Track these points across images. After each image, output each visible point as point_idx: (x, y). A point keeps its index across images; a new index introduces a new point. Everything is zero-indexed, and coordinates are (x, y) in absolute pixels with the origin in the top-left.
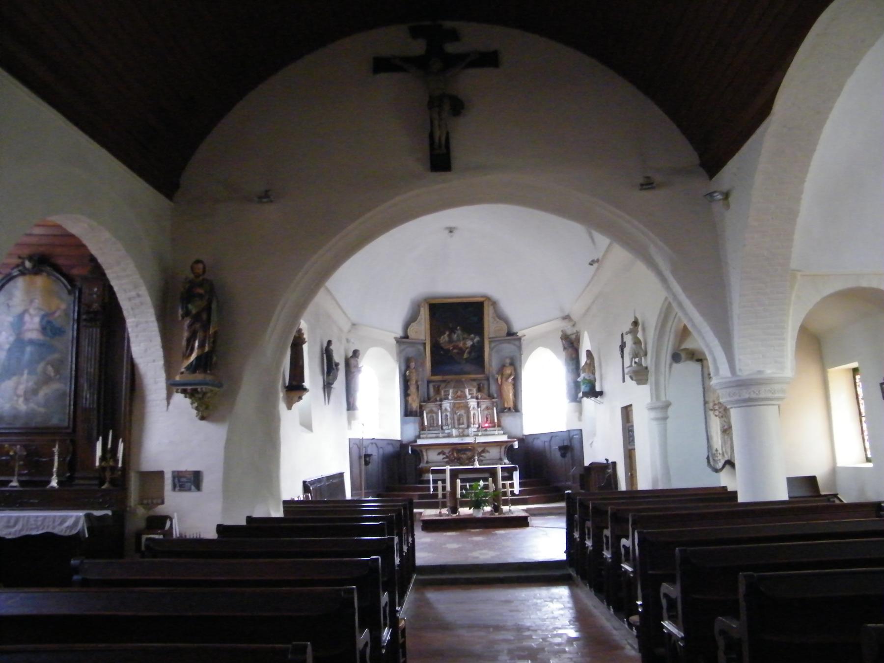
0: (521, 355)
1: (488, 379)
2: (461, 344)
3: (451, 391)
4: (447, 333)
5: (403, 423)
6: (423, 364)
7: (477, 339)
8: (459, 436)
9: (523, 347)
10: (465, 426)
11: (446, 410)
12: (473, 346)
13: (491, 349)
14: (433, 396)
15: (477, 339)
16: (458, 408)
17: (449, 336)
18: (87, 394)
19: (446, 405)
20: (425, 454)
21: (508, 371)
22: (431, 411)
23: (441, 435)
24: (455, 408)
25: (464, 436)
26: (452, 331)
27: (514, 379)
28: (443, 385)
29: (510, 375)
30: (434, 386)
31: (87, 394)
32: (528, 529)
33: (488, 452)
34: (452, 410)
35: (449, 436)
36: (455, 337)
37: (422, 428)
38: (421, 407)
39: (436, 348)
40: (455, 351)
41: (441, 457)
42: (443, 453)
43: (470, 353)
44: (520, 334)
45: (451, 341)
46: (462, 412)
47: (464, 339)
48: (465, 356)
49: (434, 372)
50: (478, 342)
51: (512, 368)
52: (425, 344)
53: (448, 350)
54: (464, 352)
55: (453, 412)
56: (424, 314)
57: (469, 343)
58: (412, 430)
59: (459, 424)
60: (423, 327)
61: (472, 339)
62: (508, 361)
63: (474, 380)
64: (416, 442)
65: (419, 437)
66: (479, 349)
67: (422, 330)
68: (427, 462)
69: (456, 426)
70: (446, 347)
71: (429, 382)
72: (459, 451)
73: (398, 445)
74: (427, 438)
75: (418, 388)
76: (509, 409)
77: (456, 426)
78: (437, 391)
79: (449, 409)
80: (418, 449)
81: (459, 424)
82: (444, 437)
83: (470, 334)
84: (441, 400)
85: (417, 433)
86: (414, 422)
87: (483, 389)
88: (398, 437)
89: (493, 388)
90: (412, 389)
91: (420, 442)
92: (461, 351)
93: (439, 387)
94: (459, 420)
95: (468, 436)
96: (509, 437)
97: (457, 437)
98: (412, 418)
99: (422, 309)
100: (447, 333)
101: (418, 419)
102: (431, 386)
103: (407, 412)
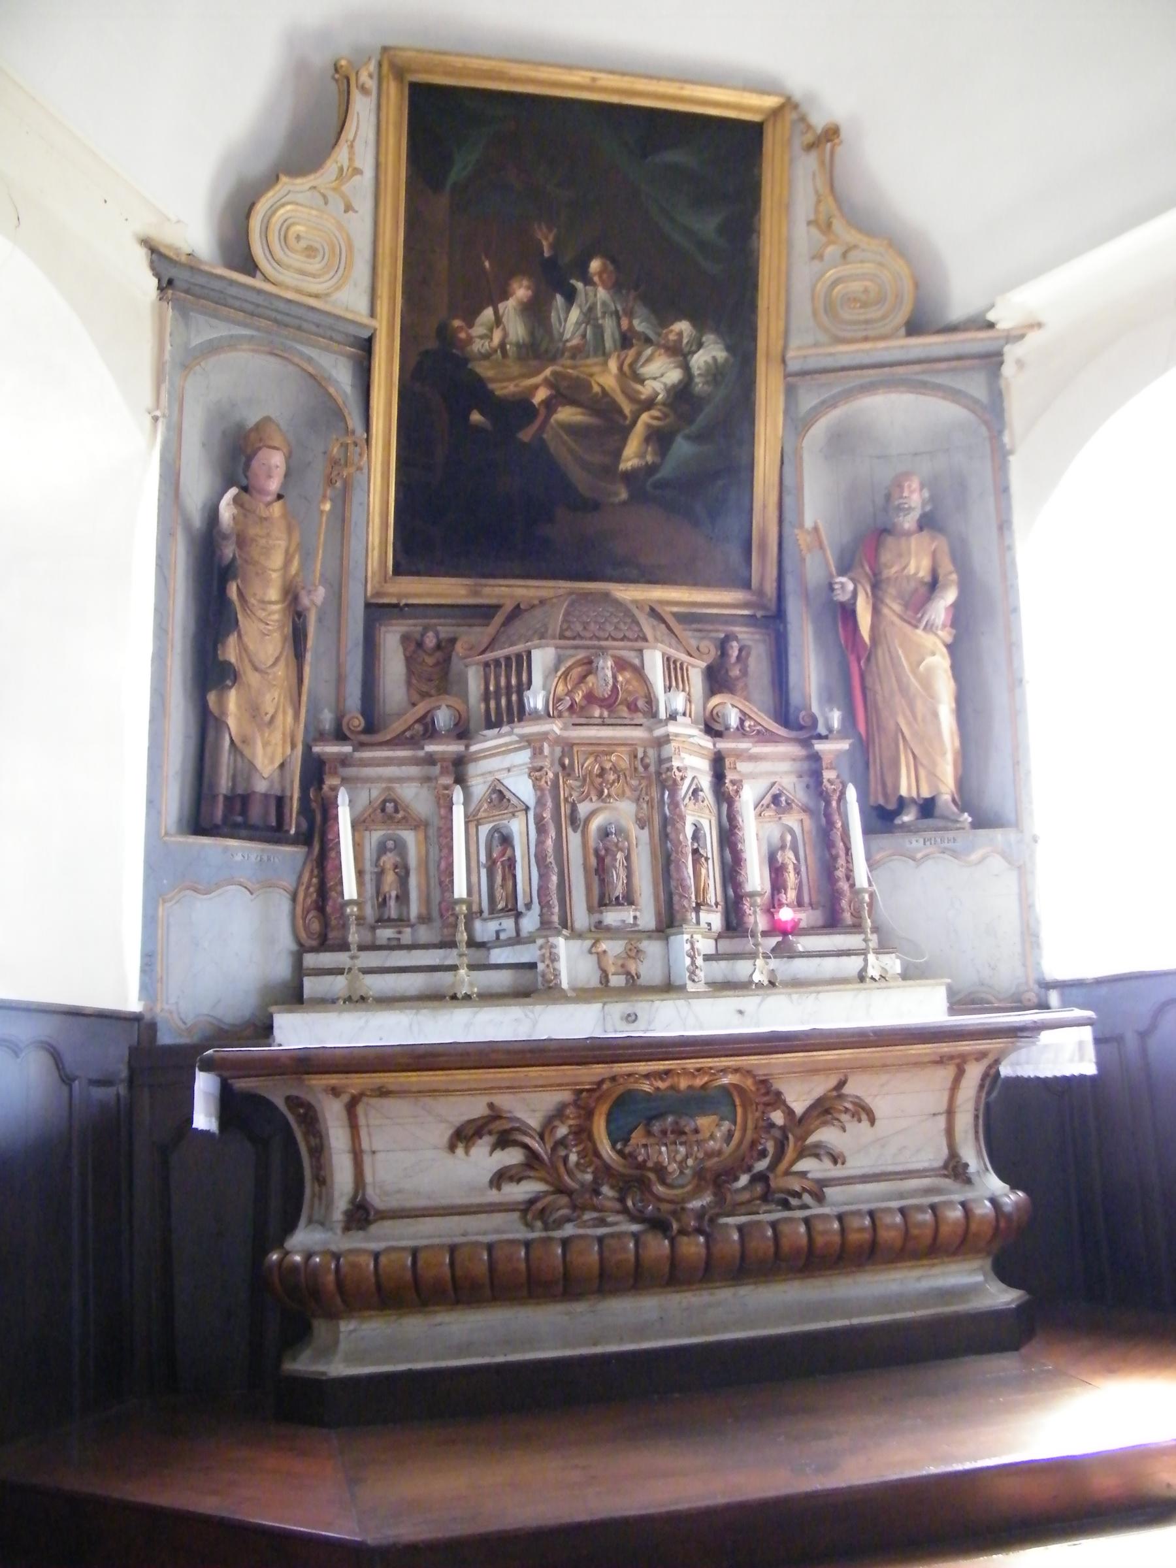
0: (1000, 456)
1: (773, 620)
2: (606, 377)
3: (542, 658)
4: (521, 291)
5: (164, 882)
6: (342, 483)
7: (711, 353)
8: (600, 991)
9: (1017, 407)
10: (646, 915)
11: (500, 797)
12: (682, 394)
13: (798, 424)
14: (432, 697)
15: (711, 353)
16: (599, 785)
17: (535, 311)
18: (445, 1059)
19: (506, 763)
20: (338, 1138)
21: (915, 560)
22: (388, 811)
23: (466, 980)
24: (570, 777)
25: (634, 987)
26: (557, 279)
27: (960, 617)
28: (473, 635)
29: (933, 585)
30: (413, 646)
31: (445, 1059)
32: (158, 1019)
33: (864, 1112)
34: (549, 792)
35: (532, 986)
36: (569, 322)
37: (321, 921)
38: (315, 771)
39: (440, 389)
40: (566, 414)
41: (484, 1160)
42: (495, 1129)
43: (660, 439)
44: (1005, 316)
45: (538, 349)
46: (622, 811)
47: (626, 340)
48: (633, 454)
49: (416, 547)
50: (716, 373)
51: (941, 544)
52: (366, 346)
53: (522, 409)
54: (625, 432)
55: (557, 814)
56: (371, 142)
57: (661, 374)
58: (237, 934)
59: (602, 900)
60: (360, 226)
61: (680, 353)
62: (915, 498)
63: (691, 619)
64: (266, 1030)
65: (293, 996)
66: (716, 421)
67: (344, 244)
68: (361, 1215)
69: (581, 917)
70: (505, 389)
71: (378, 612)
72: (632, 1111)
73: (114, 1057)
74: (357, 1001)
75: (298, 639)
76: (927, 808)
77: (581, 917)
78: (434, 671)
79: (522, 788)
80: (276, 1093)
81: (602, 900)
82: (489, 997)
83: (664, 313)
84: (462, 732)
85: (282, 969)
86: (262, 885)
87: (745, 668)
88: (114, 983)
89: (810, 673)
90: (259, 639)
91: (295, 1032)
92: (610, 422)
93: (446, 647)
94: (600, 870)
95: (669, 987)
96: (959, 1002)
97: (583, 995)
98: (240, 852)
99: (362, 108)
100: (521, 291)
101: (288, 858)
102: (391, 641)
103: (213, 804)
